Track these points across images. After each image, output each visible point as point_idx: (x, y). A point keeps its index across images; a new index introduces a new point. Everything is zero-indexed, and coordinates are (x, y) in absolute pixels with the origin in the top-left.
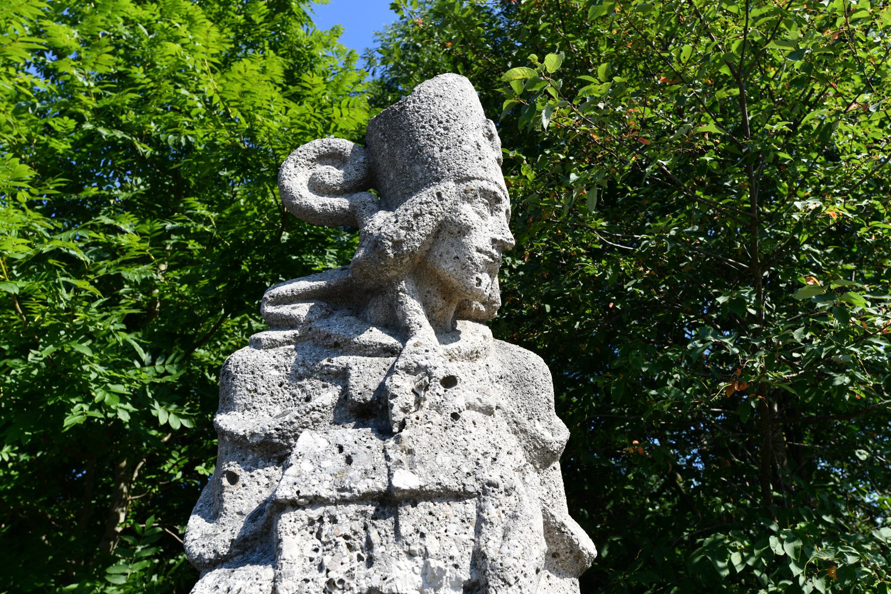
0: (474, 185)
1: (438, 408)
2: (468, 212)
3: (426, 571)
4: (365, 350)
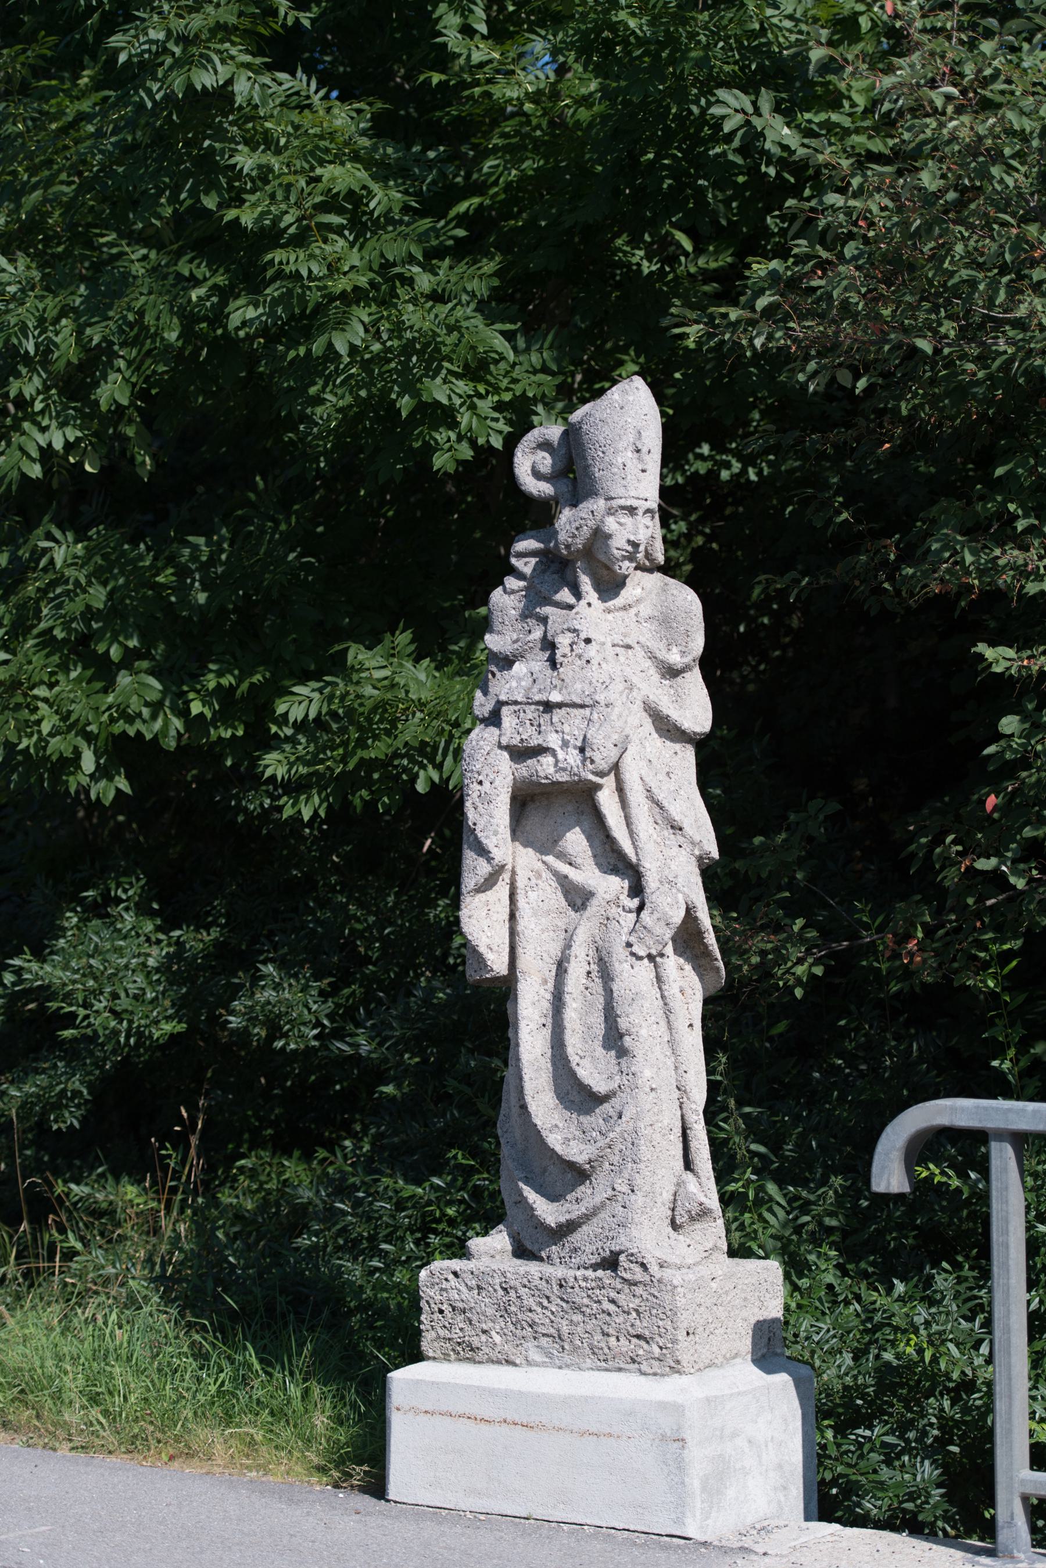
0: (615, 503)
1: (580, 657)
3: (563, 740)
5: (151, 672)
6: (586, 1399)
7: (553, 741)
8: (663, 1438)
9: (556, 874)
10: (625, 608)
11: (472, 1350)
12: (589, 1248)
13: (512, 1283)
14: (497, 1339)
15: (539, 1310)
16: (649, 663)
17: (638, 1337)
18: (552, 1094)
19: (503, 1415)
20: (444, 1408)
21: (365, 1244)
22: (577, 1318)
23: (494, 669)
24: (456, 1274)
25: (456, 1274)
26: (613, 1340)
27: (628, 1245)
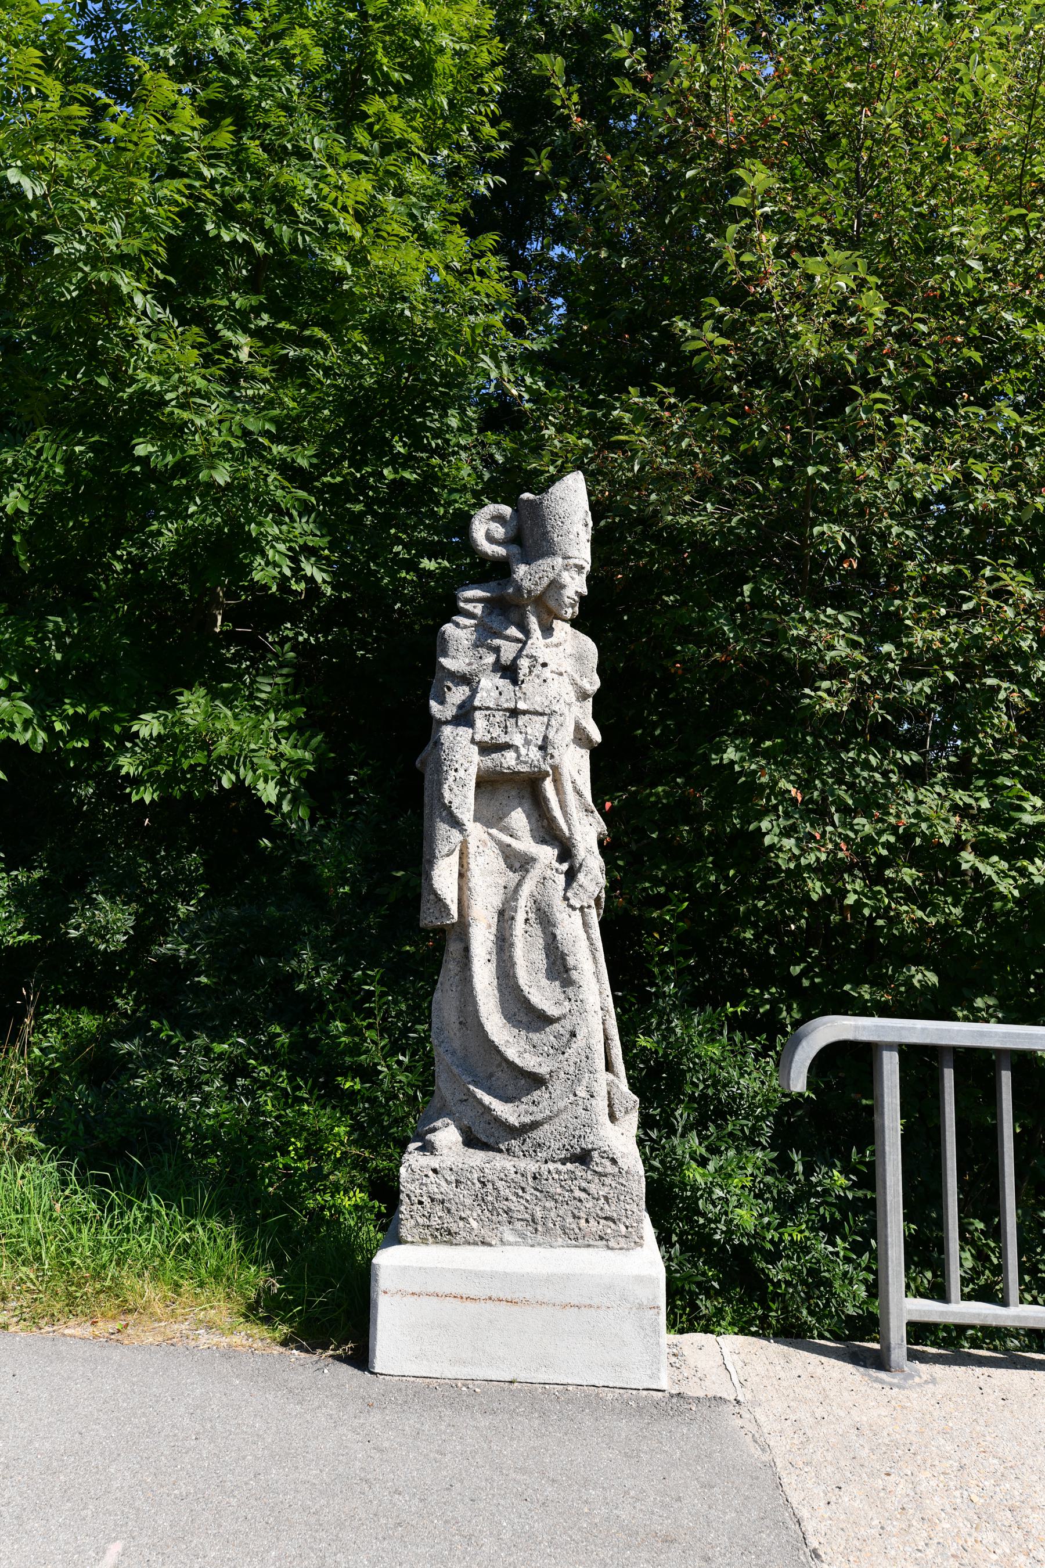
0: (572, 561)
1: (538, 677)
2: (566, 577)
3: (526, 739)
4: (508, 638)
5: (25, 699)
6: (568, 1277)
7: (518, 740)
8: (640, 1307)
9: (499, 843)
10: (557, 645)
11: (450, 1234)
12: (554, 1145)
13: (490, 1177)
14: (474, 1224)
15: (514, 1199)
16: (570, 688)
17: (606, 1218)
18: (500, 1015)
19: (489, 1293)
20: (431, 1290)
21: (185, 1084)
22: (550, 1204)
23: (450, 684)
24: (435, 1171)
25: (435, 1171)
26: (582, 1222)
27: (601, 1144)
